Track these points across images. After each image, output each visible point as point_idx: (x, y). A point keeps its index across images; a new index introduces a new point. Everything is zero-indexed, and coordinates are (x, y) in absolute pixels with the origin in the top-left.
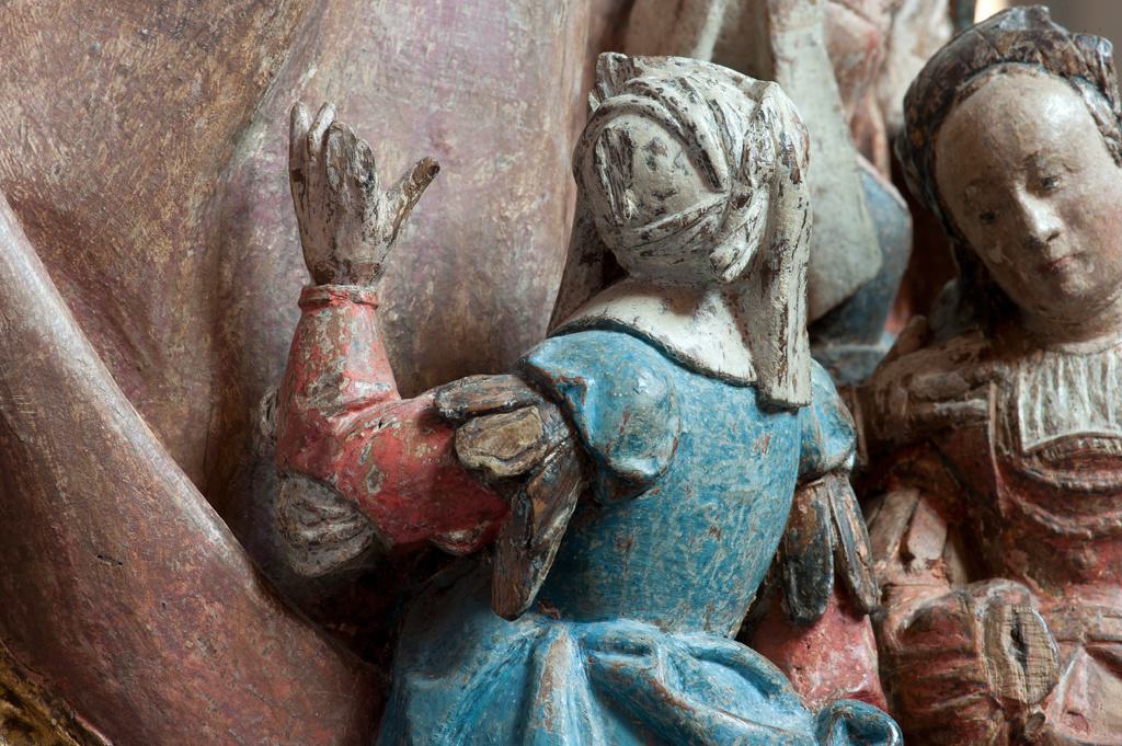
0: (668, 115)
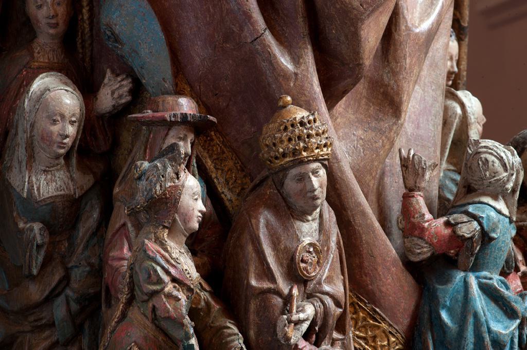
0: (496, 154)
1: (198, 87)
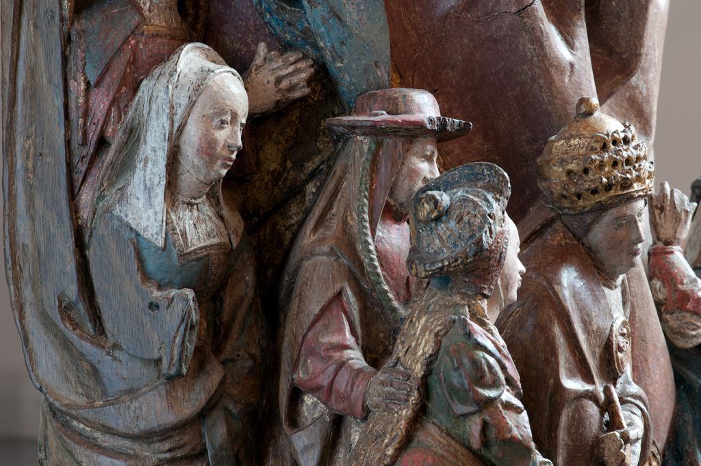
1: (410, 79)
